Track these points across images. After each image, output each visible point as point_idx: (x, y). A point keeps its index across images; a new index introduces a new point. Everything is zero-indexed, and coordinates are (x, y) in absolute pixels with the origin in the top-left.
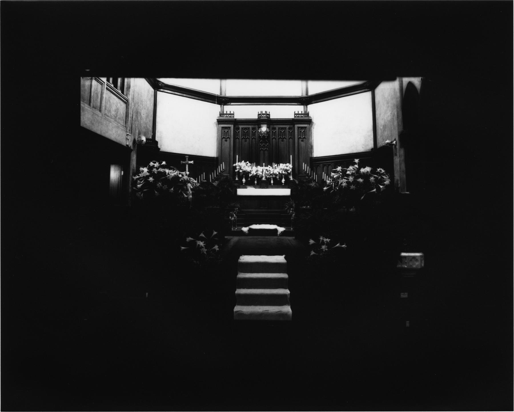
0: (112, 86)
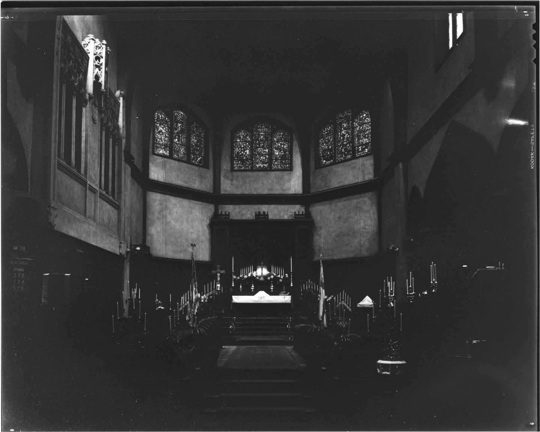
0: (104, 192)
